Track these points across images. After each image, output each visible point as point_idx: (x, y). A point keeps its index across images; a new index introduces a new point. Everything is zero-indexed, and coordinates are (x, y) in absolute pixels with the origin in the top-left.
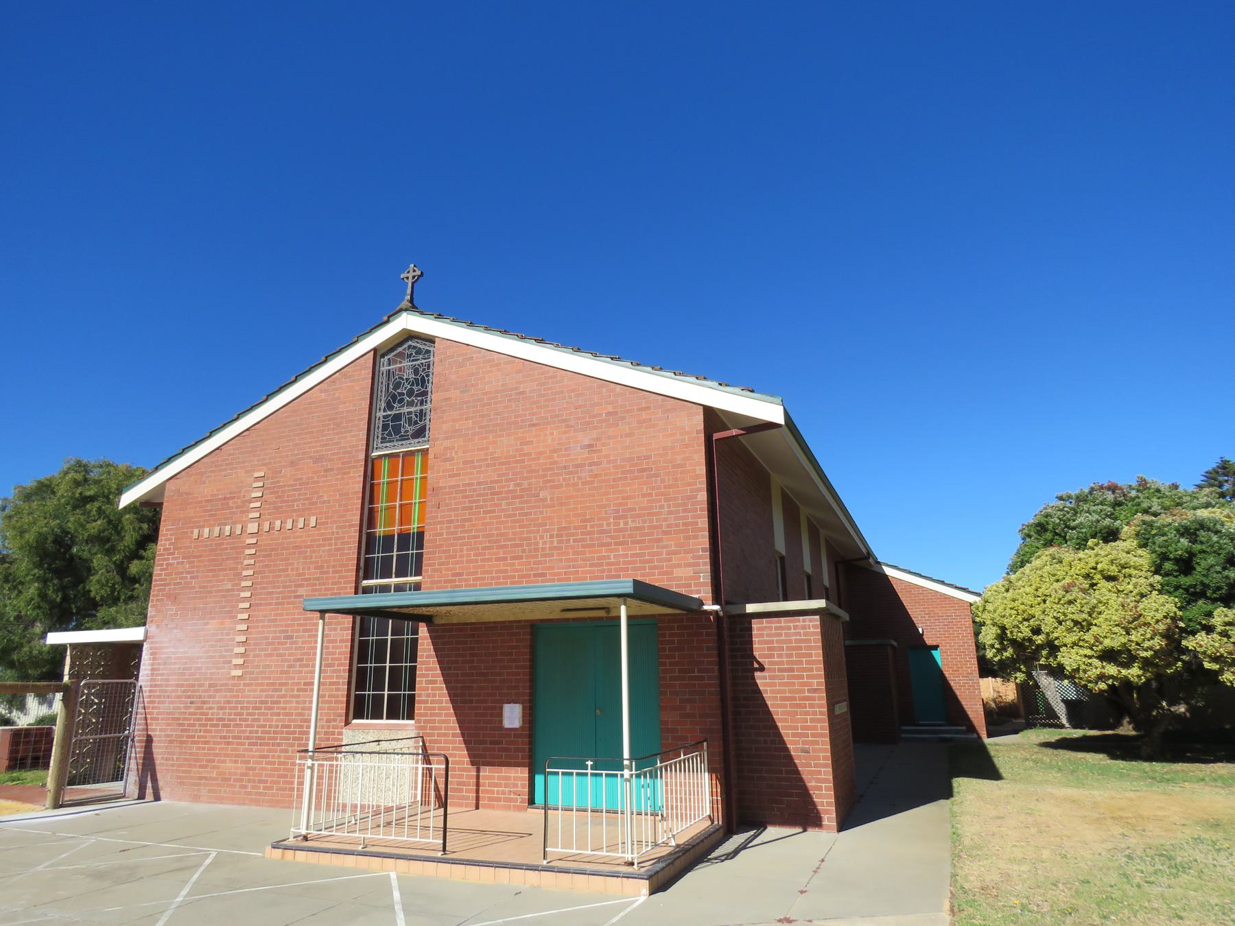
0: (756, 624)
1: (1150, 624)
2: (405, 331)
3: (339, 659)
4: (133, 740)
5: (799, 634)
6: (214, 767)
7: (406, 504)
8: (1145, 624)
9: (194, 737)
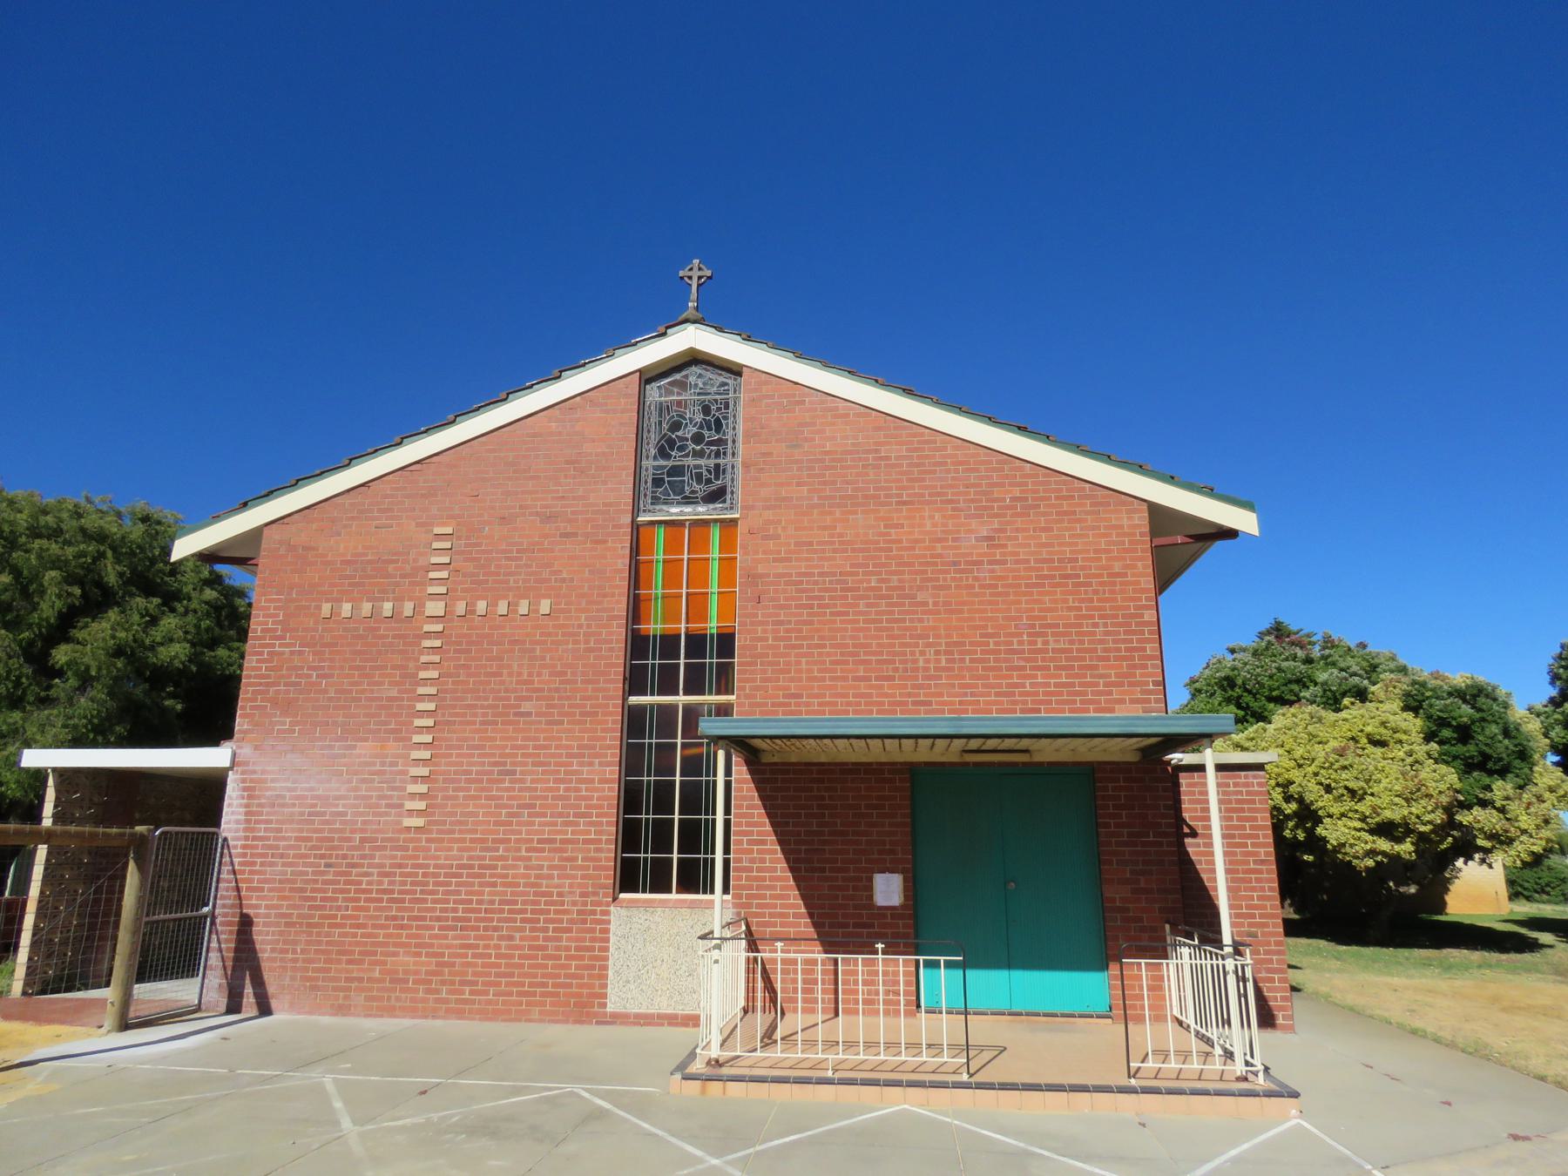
1: (1432, 796)
2: (692, 351)
3: (600, 807)
4: (213, 923)
5: (1241, 793)
6: (375, 963)
7: (696, 594)
8: (1427, 796)
9: (335, 917)
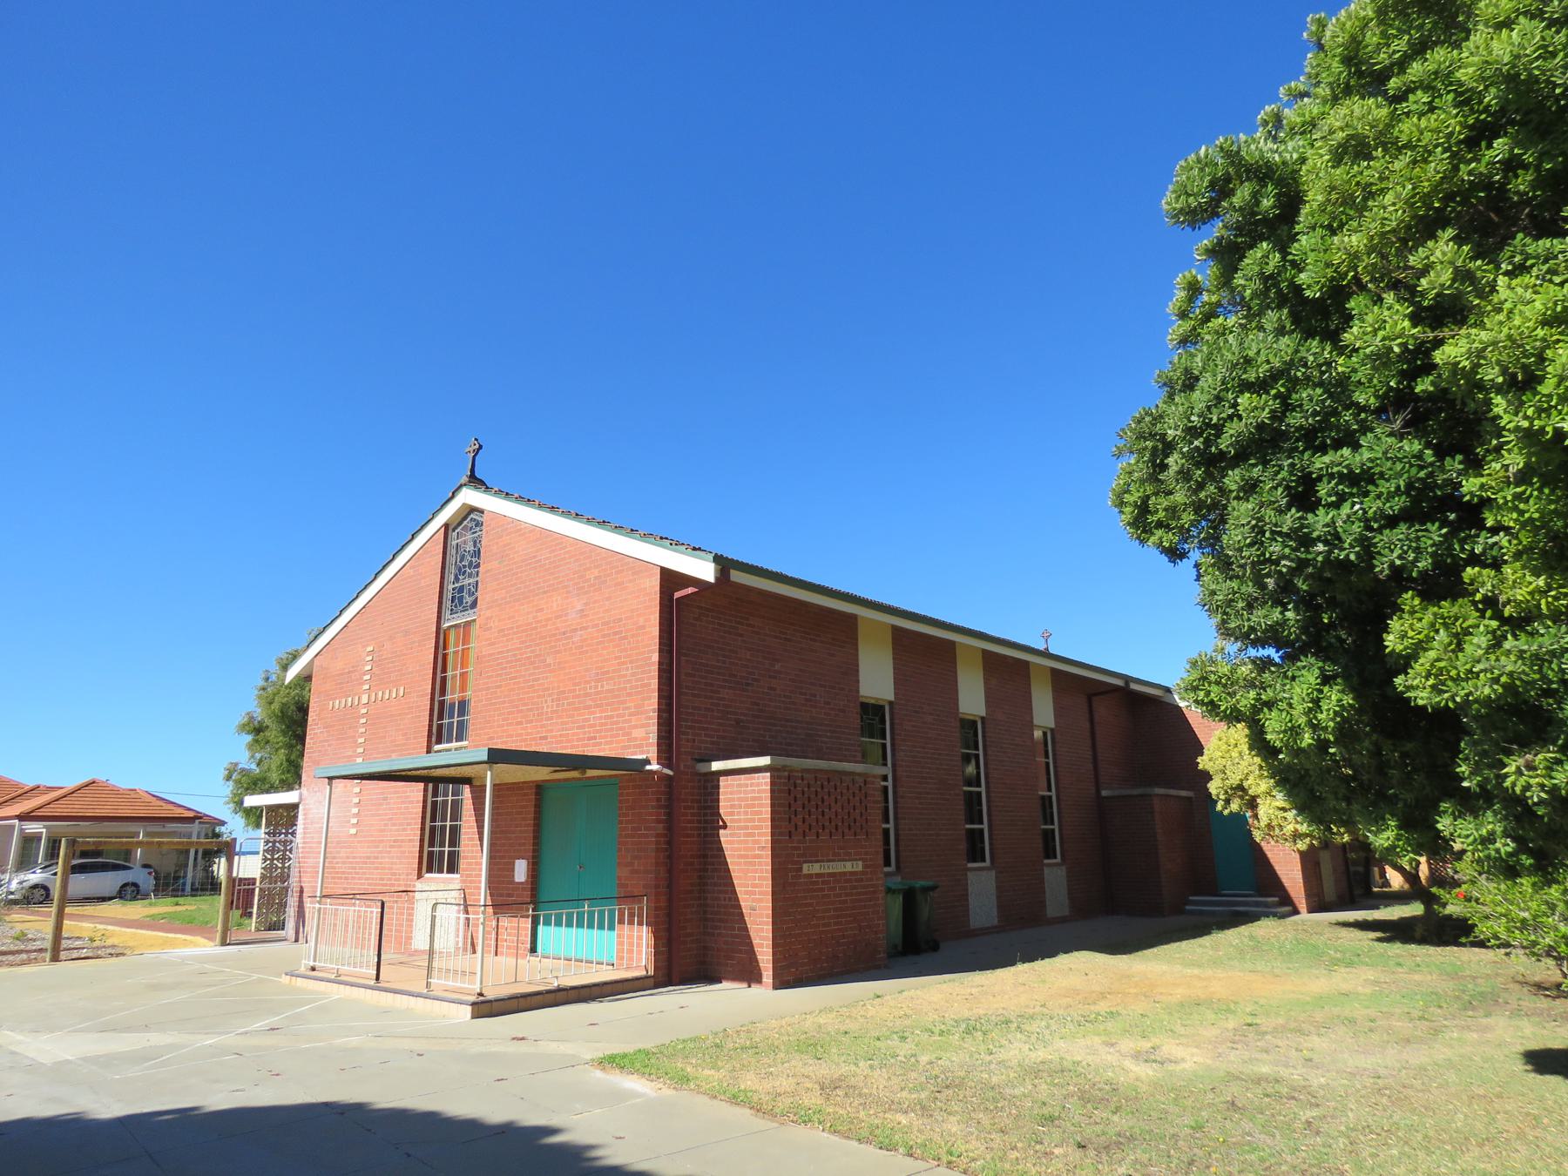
0: (723, 781)
